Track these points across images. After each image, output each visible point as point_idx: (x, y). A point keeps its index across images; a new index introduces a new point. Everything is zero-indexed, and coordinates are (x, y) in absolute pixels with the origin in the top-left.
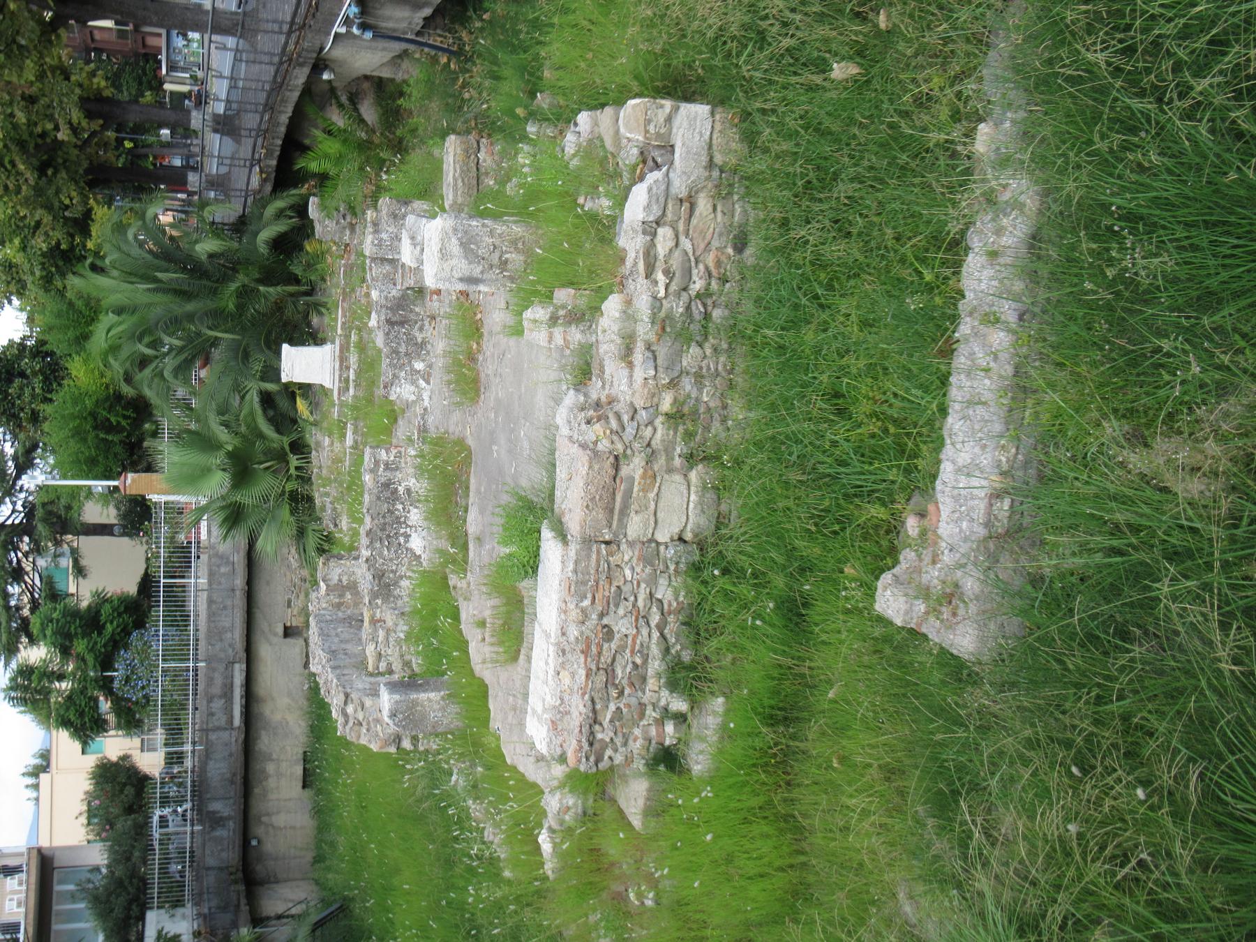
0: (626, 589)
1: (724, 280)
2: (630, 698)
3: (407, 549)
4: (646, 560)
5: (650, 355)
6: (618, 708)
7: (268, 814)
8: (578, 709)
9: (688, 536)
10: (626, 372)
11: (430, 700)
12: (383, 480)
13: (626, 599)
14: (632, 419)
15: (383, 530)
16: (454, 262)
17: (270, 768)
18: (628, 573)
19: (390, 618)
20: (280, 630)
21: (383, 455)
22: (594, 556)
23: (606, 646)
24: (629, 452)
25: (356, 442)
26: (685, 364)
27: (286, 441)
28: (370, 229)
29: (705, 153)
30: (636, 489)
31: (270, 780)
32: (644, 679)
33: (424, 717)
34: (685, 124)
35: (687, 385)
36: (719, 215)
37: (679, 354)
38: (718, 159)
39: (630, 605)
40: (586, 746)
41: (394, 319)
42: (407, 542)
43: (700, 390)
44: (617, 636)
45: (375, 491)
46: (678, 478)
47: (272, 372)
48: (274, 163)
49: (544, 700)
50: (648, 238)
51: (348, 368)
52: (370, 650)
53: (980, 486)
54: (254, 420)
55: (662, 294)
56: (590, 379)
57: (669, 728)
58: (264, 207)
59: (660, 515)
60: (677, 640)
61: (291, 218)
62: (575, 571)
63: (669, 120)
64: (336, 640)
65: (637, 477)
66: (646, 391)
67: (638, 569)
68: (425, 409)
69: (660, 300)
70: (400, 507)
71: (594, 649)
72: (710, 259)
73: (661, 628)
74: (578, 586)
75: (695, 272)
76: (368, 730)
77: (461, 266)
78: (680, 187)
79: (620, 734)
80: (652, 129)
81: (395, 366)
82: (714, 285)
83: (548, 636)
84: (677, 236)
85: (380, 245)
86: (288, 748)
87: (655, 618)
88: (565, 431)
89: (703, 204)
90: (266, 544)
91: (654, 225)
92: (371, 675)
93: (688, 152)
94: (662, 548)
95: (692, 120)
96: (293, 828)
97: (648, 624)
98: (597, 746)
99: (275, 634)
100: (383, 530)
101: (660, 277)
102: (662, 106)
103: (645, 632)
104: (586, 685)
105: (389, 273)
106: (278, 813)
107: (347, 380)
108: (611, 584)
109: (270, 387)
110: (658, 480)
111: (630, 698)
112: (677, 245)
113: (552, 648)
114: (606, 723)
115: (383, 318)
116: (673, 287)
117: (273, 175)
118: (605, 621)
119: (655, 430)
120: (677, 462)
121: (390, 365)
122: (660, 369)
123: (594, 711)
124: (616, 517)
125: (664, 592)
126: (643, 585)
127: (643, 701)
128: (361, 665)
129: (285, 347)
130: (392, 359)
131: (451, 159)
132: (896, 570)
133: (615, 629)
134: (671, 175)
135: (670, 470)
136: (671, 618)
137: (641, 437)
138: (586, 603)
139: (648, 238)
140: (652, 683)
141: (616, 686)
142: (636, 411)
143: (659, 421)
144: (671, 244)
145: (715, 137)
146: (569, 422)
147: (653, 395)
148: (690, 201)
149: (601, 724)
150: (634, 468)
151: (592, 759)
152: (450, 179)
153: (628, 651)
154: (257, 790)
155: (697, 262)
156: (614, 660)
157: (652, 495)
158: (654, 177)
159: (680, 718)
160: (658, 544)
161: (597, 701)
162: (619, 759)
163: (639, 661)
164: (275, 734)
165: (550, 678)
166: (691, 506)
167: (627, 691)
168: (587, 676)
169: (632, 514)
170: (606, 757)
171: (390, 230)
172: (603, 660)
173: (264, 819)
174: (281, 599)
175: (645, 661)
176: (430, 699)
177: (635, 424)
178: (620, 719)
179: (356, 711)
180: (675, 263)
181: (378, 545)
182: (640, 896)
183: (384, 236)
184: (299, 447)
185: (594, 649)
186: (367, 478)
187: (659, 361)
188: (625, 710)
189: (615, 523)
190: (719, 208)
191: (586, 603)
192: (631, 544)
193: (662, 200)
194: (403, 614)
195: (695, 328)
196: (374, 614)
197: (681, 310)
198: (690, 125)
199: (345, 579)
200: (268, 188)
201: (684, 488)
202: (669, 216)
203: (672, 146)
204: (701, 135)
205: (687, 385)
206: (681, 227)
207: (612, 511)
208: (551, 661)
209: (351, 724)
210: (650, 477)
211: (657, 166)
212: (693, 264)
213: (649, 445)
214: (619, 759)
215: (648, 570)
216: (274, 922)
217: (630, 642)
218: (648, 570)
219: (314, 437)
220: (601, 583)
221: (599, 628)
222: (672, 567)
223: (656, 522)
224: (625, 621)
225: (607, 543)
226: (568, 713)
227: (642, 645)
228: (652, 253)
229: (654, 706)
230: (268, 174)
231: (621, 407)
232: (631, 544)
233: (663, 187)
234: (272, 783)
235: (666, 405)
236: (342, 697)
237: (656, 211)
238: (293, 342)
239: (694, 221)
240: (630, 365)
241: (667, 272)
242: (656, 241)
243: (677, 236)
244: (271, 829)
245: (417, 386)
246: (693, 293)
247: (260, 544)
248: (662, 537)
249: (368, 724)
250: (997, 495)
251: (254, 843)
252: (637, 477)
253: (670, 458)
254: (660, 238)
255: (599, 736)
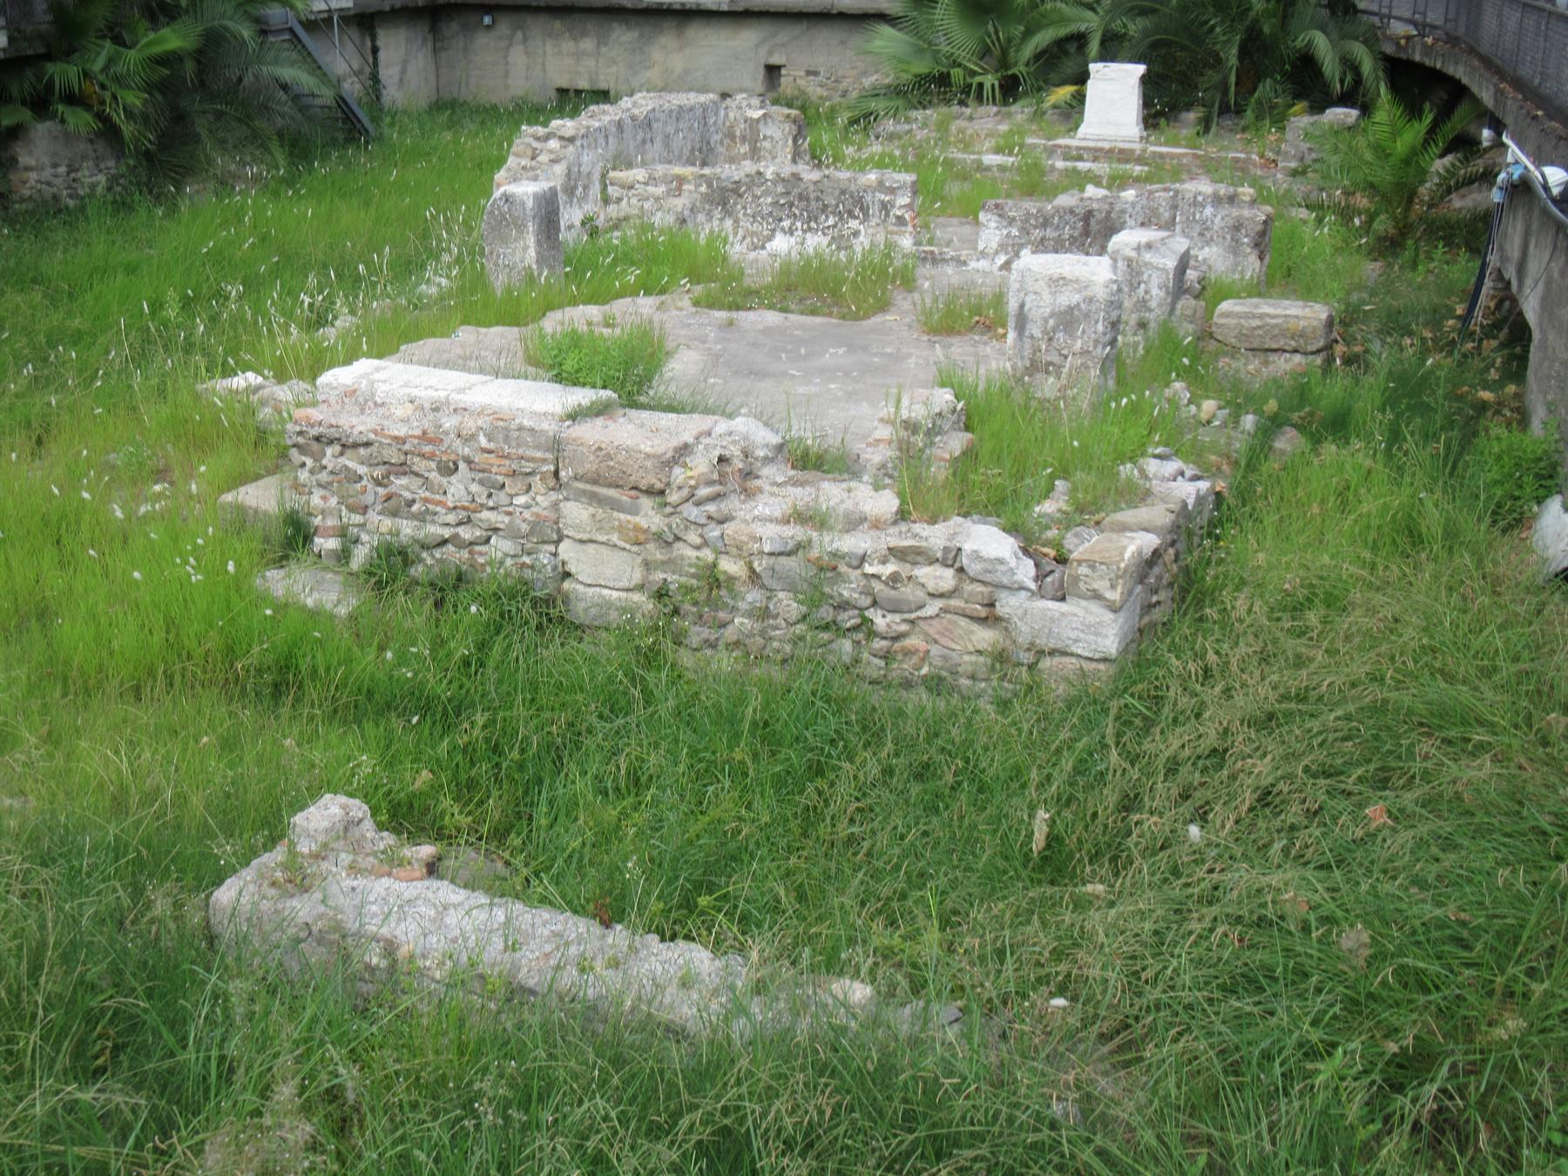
0: (501, 497)
1: (887, 656)
2: (373, 494)
3: (774, 231)
4: (536, 526)
5: (791, 545)
6: (361, 478)
7: (525, 40)
8: (358, 424)
9: (567, 585)
10: (778, 513)
11: (526, 248)
12: (868, 198)
13: (490, 495)
14: (710, 518)
15: (801, 197)
16: (1047, 296)
17: (588, 44)
18: (521, 500)
19: (680, 203)
20: (776, 60)
21: (903, 200)
22: (539, 455)
23: (433, 465)
24: (668, 510)
25: (988, 169)
26: (781, 595)
27: (1020, 69)
28: (1223, 190)
29: (1052, 644)
30: (622, 516)
31: (571, 43)
32: (395, 514)
33: (505, 240)
34: (1091, 619)
35: (753, 596)
36: (974, 658)
37: (792, 589)
38: (1046, 663)
39: (482, 499)
40: (314, 432)
41: (1093, 222)
42: (783, 229)
43: (749, 614)
44: (444, 481)
45: (853, 187)
46: (637, 577)
47: (1112, 49)
48: (1417, 58)
49: (384, 382)
50: (939, 555)
51: (1095, 160)
52: (639, 174)
53: (407, 933)
54: (1052, 23)
55: (868, 569)
56: (793, 467)
57: (331, 544)
58: (1365, 42)
59: (591, 548)
60: (438, 561)
61: (1342, 81)
62: (521, 428)
63: (1097, 596)
64: (670, 130)
65: (637, 519)
66: (744, 538)
67: (527, 515)
68: (965, 263)
69: (860, 566)
70: (831, 221)
71: (427, 449)
72: (913, 642)
73: (454, 539)
74: (503, 429)
75: (897, 617)
76: (524, 168)
77: (1042, 305)
78: (1009, 605)
79: (331, 478)
80: (1083, 570)
81: (1026, 221)
82: (879, 644)
83: (460, 391)
84: (942, 596)
85: (1195, 203)
86: (614, 69)
87: (466, 533)
88: (722, 426)
89: (985, 637)
90: (886, 39)
91: (957, 565)
92: (604, 176)
93: (1052, 620)
94: (552, 548)
95: (1095, 629)
96: (507, 74)
97: (460, 524)
98: (315, 446)
99: (770, 53)
100: (801, 197)
101: (890, 568)
102: (1113, 587)
103: (451, 518)
104: (386, 437)
105: (1158, 216)
106: (527, 53)
107: (1080, 158)
108: (507, 475)
109: (1094, 46)
110: (635, 548)
111: (373, 494)
112: (931, 595)
113: (442, 394)
114: (343, 461)
115: (1095, 206)
116: (877, 586)
117: (1403, 56)
118: (462, 466)
119: (698, 548)
120: (659, 576)
121: (1028, 215)
122: (772, 560)
123: (356, 446)
124: (588, 487)
125: (501, 546)
126: (507, 519)
127: (370, 511)
128: (623, 161)
129: (1141, 69)
130: (1036, 218)
131: (1293, 312)
132: (368, 824)
133: (453, 479)
134: (1023, 594)
135: (647, 565)
136: (465, 554)
137: (686, 528)
138: (483, 441)
139: (939, 555)
140: (387, 523)
141: (387, 476)
142: (721, 522)
143: (707, 555)
144: (931, 586)
145: (1074, 660)
146: (730, 434)
147: (739, 548)
148: (990, 617)
149: (342, 454)
150: (649, 517)
151: (300, 440)
152: (1266, 309)
153: (428, 494)
154: (558, 24)
155: (912, 622)
156: (417, 475)
157: (615, 538)
158: (1025, 571)
159: (344, 556)
160: (557, 542)
161: (369, 450)
162: (303, 476)
163: (415, 508)
164: (634, 51)
165: (408, 390)
166: (606, 592)
167: (381, 491)
168: (396, 438)
169: (592, 510)
170: (304, 458)
171: (1217, 221)
172: (416, 459)
173: (519, 34)
174: (819, 60)
175: (414, 517)
176: (526, 250)
177: (703, 521)
178: (348, 480)
179: (551, 151)
180: (907, 592)
181: (780, 189)
182: (158, 497)
183: (1208, 211)
184: (1010, 89)
185: (427, 449)
186: (872, 177)
187: (782, 559)
188: (358, 486)
189: (581, 485)
190: (981, 659)
191: (483, 441)
192: (555, 506)
193: (988, 577)
194: (684, 221)
195: (826, 613)
196: (689, 182)
197: (845, 593)
198: (1089, 626)
199: (767, 144)
200: (1389, 49)
201: (625, 583)
202: (969, 587)
203: (1063, 599)
204: (1076, 641)
205: (753, 596)
206: (954, 603)
207: (595, 482)
208: (431, 393)
209: (535, 144)
210: (640, 538)
211: (1040, 577)
212: (907, 616)
213: (678, 539)
214: (303, 476)
215: (525, 527)
216: (369, 44)
217: (438, 497)
218: (525, 527)
219: (1020, 111)
220: (508, 462)
221: (453, 457)
222: (527, 560)
223: (582, 542)
224: (463, 492)
225: (556, 473)
226: (362, 411)
227: (436, 514)
228: (919, 559)
229: (362, 526)
230: (1404, 49)
231: (733, 504)
232: (555, 506)
233: (1005, 581)
234: (568, 46)
235: (729, 566)
236: (569, 133)
237: (973, 568)
238: (1145, 80)
239: (963, 622)
240: (786, 521)
241: (895, 578)
242: (937, 566)
243: (942, 596)
244: (503, 44)
245: (997, 252)
246: (870, 613)
247: (886, 30)
248: (566, 549)
249: (532, 168)
250: (390, 948)
251: (487, 20)
252: (637, 519)
253: (665, 564)
254: (938, 570)
255: (329, 451)
